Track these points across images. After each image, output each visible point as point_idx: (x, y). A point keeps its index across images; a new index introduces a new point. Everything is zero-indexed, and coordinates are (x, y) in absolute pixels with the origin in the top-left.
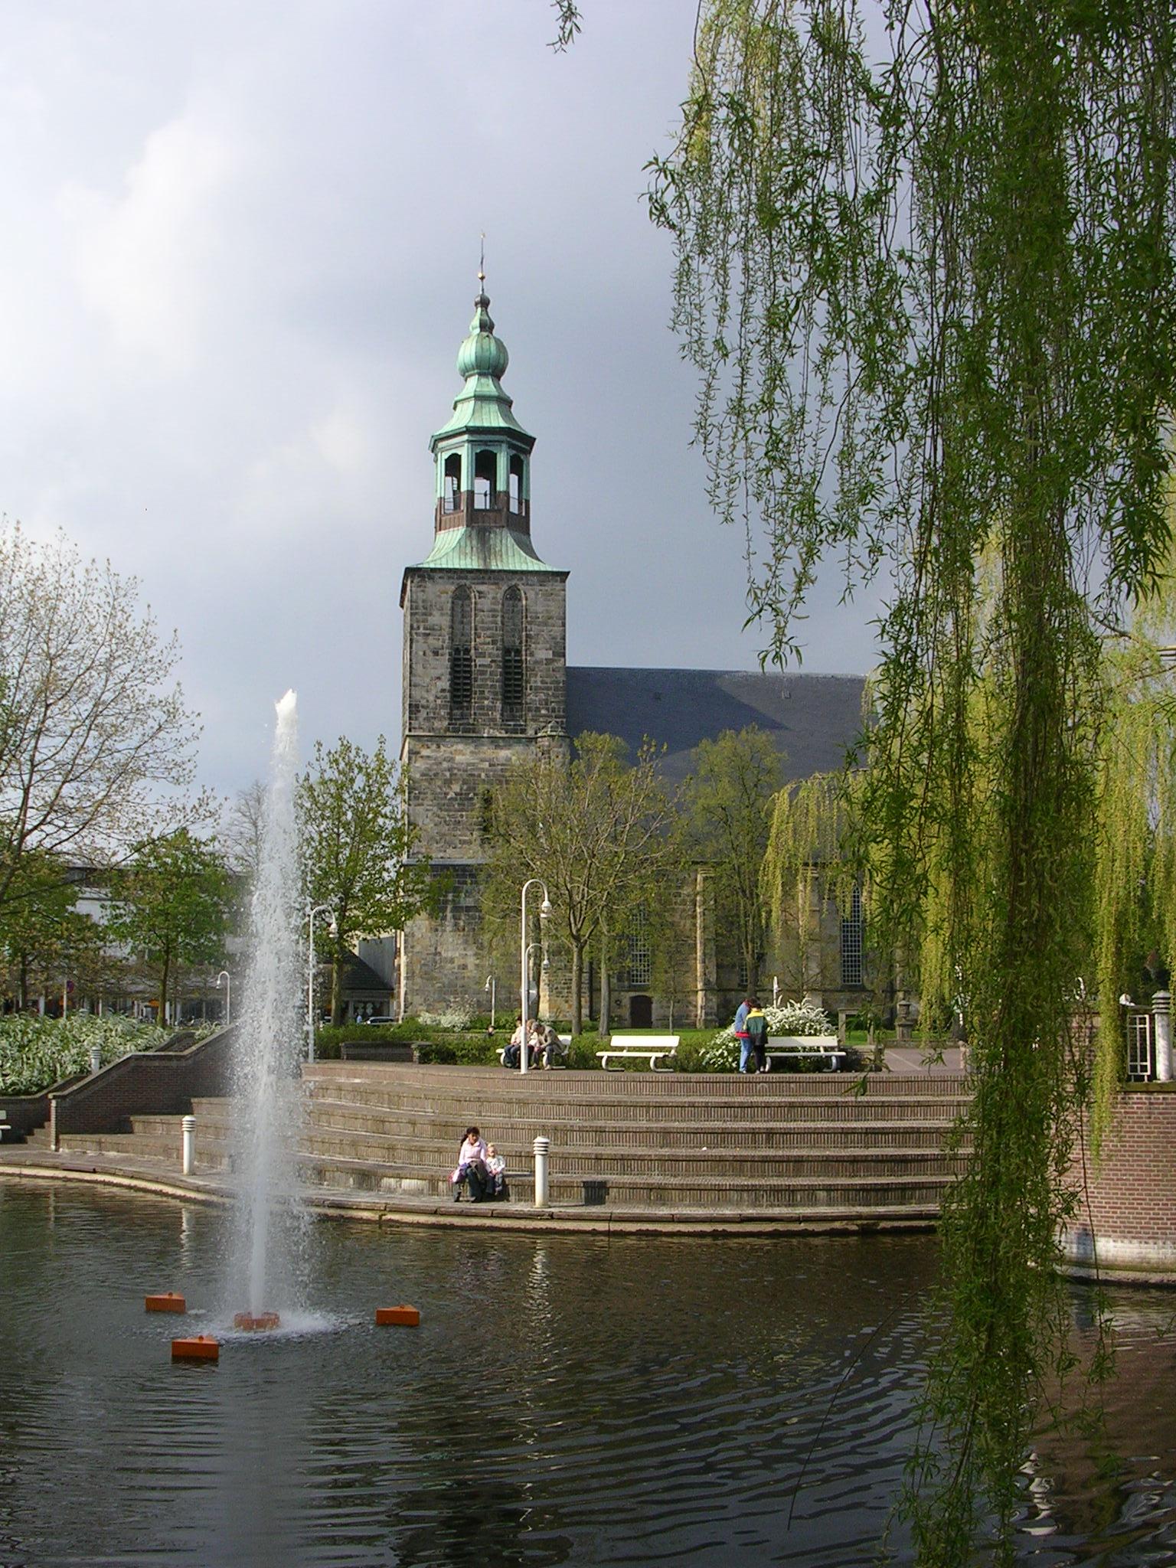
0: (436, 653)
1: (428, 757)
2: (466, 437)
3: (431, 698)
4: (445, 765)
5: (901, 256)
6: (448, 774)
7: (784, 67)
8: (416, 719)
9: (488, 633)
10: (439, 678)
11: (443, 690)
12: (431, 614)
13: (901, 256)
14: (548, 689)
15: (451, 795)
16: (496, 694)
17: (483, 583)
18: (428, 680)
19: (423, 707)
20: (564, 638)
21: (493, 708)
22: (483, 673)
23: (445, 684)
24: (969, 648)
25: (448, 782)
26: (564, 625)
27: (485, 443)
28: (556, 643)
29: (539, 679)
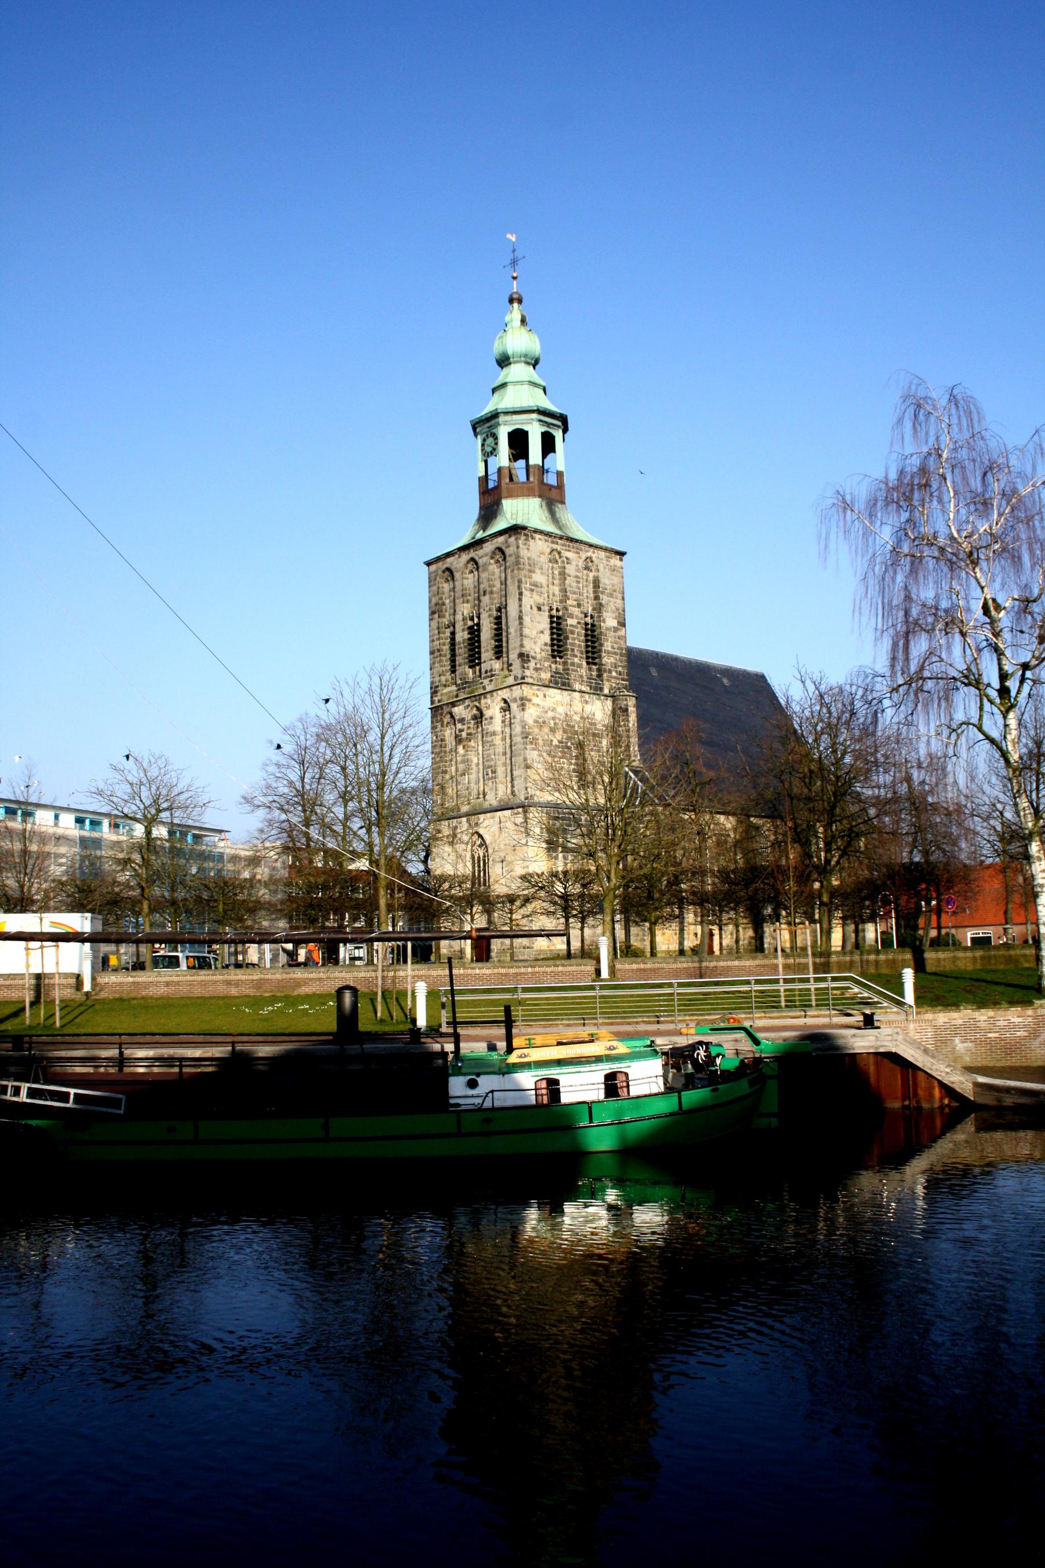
0: (539, 609)
1: (538, 705)
2: (535, 416)
3: (538, 650)
4: (550, 714)
5: (653, 1042)
6: (552, 722)
7: (975, 1306)
8: (528, 668)
9: (575, 596)
10: (542, 632)
11: (546, 644)
12: (534, 572)
13: (653, 1042)
14: (616, 653)
15: (555, 742)
16: (582, 653)
17: (569, 551)
18: (534, 632)
19: (532, 657)
20: (624, 611)
21: (580, 666)
22: (572, 632)
23: (546, 638)
24: (915, 840)
25: (553, 730)
26: (623, 599)
27: (548, 425)
28: (619, 614)
29: (609, 644)
